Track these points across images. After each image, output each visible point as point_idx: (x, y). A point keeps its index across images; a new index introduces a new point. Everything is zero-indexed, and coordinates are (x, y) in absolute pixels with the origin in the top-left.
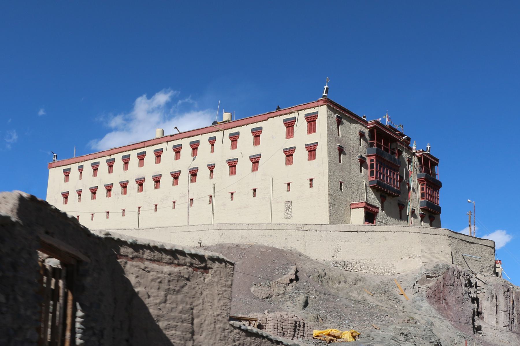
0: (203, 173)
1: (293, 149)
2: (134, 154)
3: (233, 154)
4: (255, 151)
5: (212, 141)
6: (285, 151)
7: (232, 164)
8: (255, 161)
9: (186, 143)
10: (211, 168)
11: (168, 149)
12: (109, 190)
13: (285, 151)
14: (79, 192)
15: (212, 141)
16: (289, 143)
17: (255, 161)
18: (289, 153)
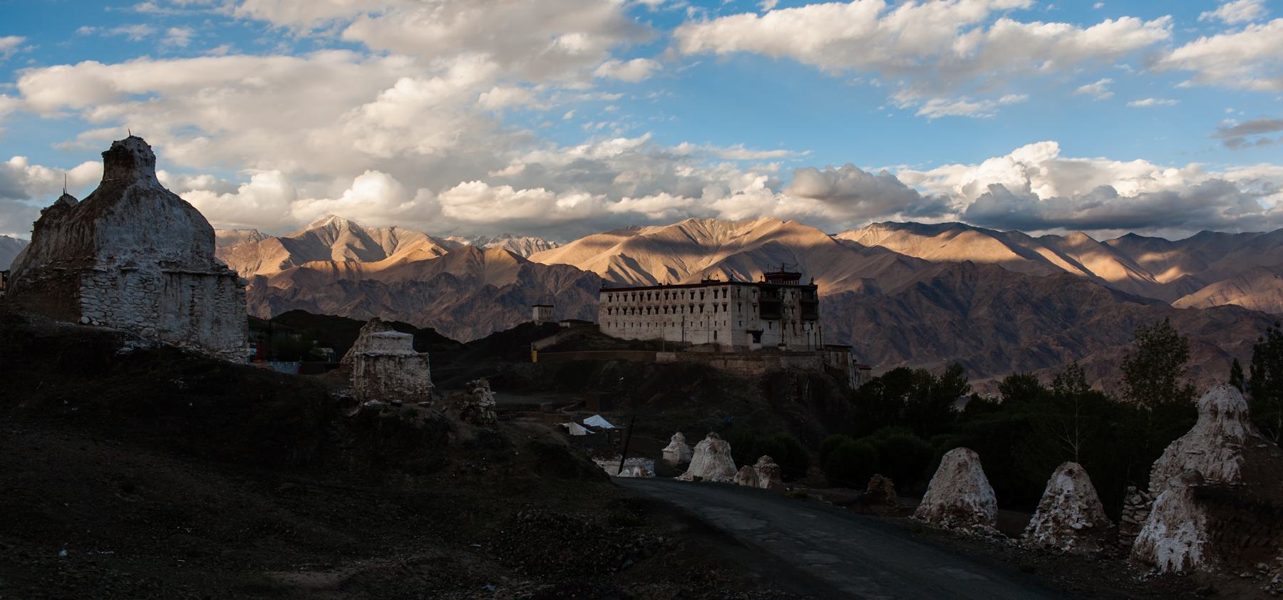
8: (702, 307)
18: (716, 306)
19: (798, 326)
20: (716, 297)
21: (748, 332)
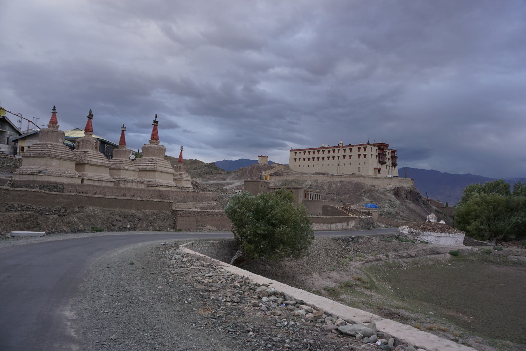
0: (336, 158)
1: (360, 155)
2: (316, 151)
3: (345, 154)
4: (350, 154)
5: (339, 150)
6: (358, 155)
7: (344, 157)
8: (350, 156)
9: (331, 150)
10: (339, 157)
11: (302, 152)
12: (318, 160)
13: (358, 155)
14: (300, 159)
15: (339, 150)
16: (359, 153)
17: (350, 156)
18: (359, 156)
19: (391, 167)
20: (359, 151)
21: (375, 169)
